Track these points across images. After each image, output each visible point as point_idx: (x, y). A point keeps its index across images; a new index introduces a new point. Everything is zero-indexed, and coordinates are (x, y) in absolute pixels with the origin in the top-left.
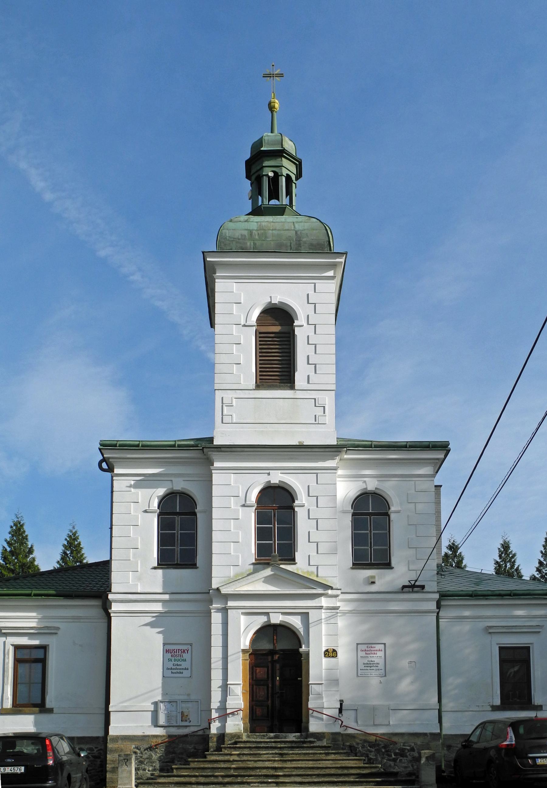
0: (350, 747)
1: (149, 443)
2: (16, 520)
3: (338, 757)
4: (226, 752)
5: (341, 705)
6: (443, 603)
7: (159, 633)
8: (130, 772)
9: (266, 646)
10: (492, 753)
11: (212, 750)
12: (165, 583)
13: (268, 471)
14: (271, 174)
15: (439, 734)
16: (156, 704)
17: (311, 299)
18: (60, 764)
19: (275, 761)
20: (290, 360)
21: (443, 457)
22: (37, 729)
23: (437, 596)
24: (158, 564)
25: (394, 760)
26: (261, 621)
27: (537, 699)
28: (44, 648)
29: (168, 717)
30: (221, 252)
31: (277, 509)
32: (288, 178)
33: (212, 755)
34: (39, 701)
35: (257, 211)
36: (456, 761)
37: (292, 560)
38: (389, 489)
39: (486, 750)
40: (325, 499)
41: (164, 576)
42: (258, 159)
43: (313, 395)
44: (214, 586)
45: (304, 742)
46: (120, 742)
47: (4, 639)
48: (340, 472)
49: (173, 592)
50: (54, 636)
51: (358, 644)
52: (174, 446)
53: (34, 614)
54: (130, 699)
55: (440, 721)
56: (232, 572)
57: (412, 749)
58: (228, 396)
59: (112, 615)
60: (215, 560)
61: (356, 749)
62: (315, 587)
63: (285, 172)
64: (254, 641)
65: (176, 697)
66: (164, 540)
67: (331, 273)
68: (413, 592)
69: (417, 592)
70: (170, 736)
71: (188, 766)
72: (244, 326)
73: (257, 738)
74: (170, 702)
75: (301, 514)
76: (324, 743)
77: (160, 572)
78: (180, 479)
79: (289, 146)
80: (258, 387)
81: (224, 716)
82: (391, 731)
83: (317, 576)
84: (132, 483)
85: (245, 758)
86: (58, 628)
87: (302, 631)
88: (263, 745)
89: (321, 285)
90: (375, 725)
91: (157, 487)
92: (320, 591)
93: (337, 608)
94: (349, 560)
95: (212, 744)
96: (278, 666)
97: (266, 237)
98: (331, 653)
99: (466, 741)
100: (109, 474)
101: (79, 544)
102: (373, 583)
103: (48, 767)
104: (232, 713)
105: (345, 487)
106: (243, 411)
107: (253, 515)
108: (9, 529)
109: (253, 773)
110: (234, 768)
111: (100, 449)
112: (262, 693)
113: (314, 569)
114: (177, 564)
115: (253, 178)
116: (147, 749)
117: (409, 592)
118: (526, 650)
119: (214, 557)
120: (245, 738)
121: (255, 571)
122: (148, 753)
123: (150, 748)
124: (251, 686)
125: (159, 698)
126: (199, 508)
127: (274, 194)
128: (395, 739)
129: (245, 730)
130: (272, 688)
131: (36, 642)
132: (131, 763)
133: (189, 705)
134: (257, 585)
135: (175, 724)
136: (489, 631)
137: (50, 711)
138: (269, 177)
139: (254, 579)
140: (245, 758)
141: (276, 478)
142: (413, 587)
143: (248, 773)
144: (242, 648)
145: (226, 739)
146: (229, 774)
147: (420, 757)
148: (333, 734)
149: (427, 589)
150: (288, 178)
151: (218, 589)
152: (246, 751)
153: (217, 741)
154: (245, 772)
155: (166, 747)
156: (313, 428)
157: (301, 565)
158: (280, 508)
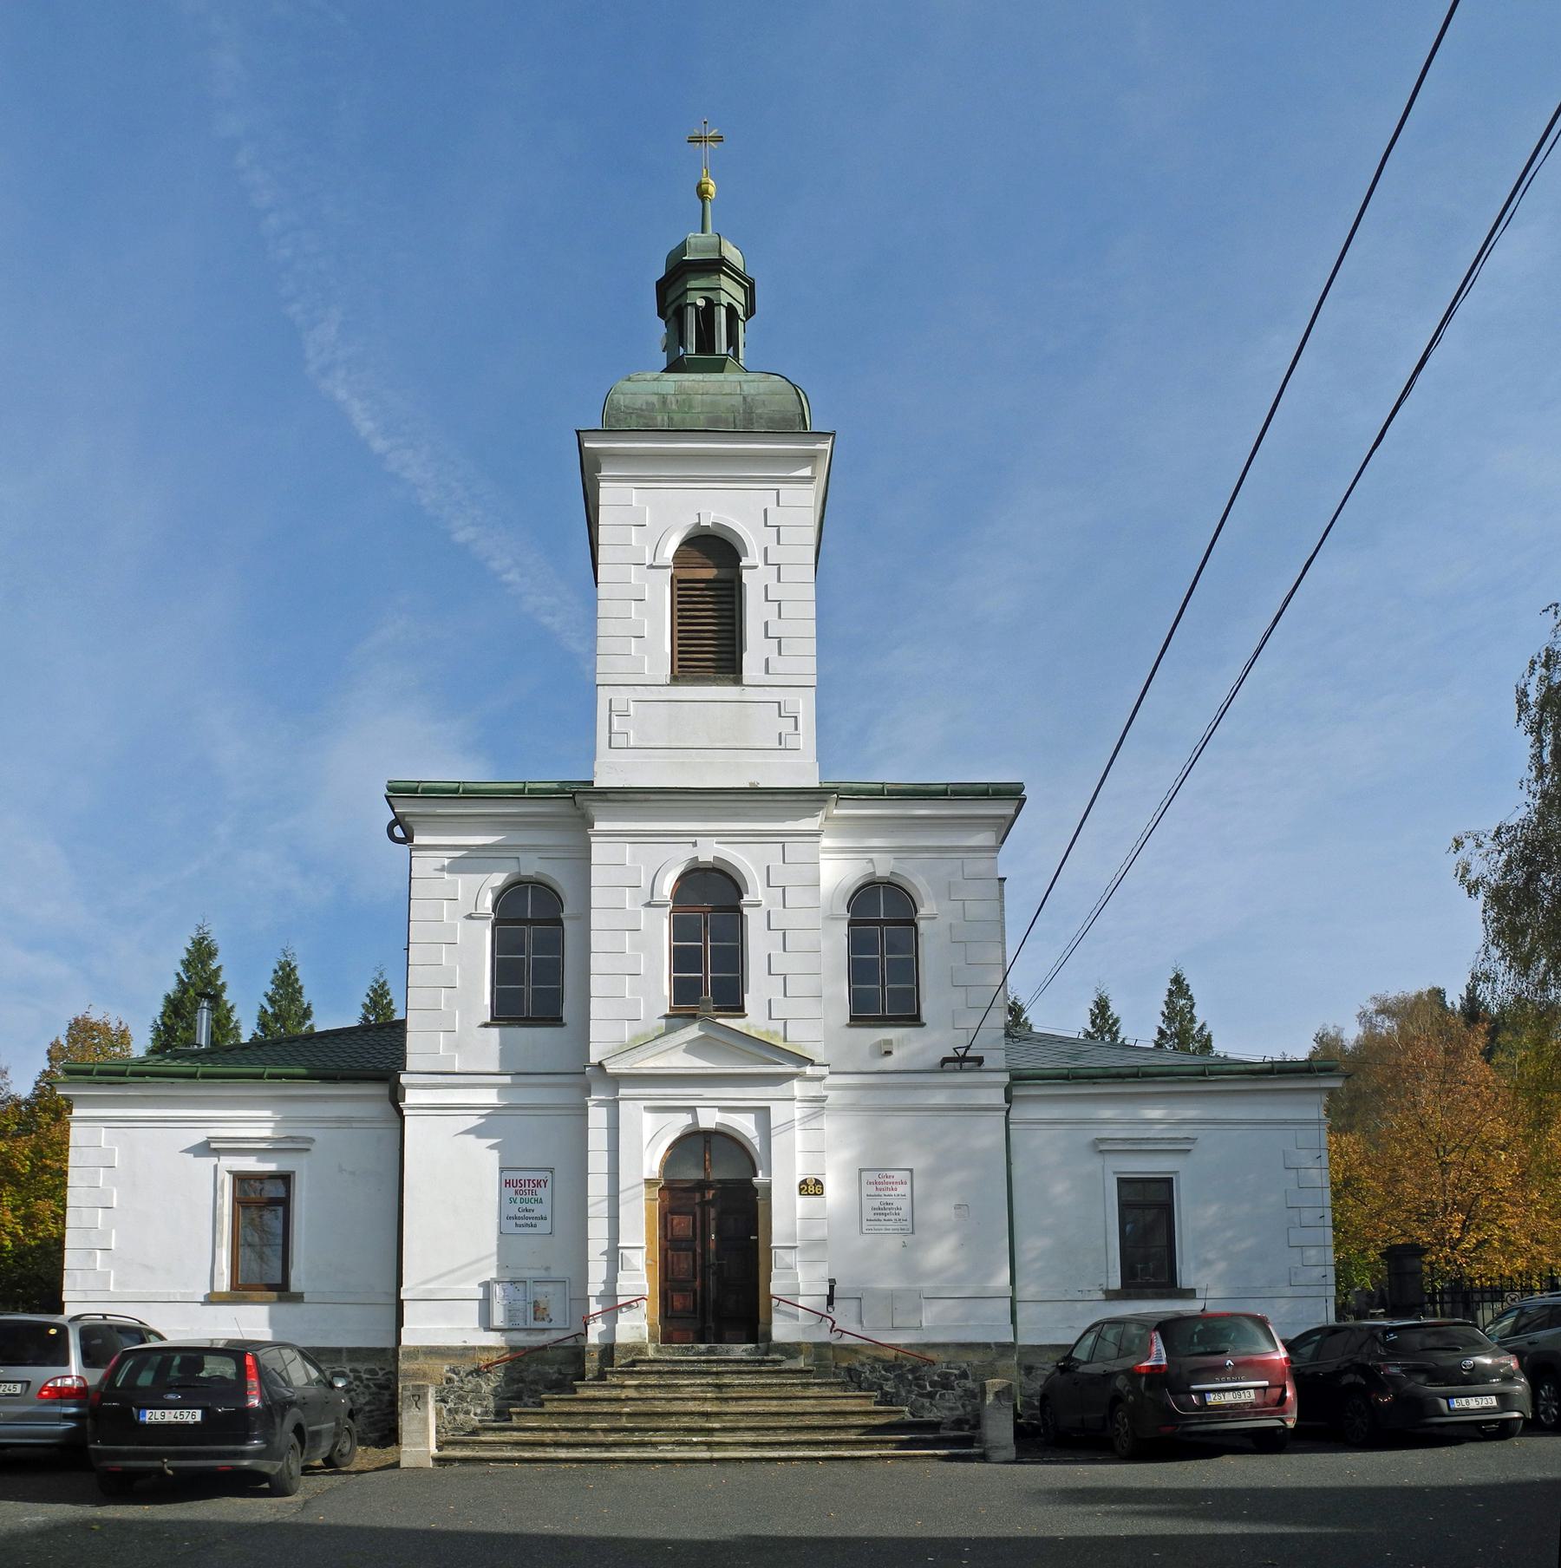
0: (849, 1370)
1: (476, 786)
2: (283, 959)
3: (827, 1392)
4: (615, 1381)
5: (832, 1288)
6: (1016, 1092)
7: (491, 1147)
8: (425, 1421)
9: (693, 1174)
10: (1121, 1383)
11: (590, 1376)
12: (505, 1053)
13: (693, 839)
14: (701, 303)
15: (1012, 1346)
16: (486, 1286)
17: (774, 520)
18: (277, 1407)
19: (706, 1399)
20: (733, 631)
21: (1012, 812)
22: (275, 1332)
23: (1005, 1078)
24: (493, 1018)
25: (931, 1396)
26: (681, 1122)
27: (1187, 1276)
28: (285, 1178)
29: (510, 1312)
30: (609, 431)
31: (710, 908)
32: (731, 310)
33: (588, 1386)
34: (278, 1280)
35: (676, 365)
36: (1044, 1398)
37: (738, 1009)
38: (920, 882)
39: (1108, 1377)
40: (800, 890)
41: (503, 1041)
42: (680, 271)
43: (776, 695)
44: (594, 1059)
45: (762, 1362)
46: (421, 1358)
47: (214, 1160)
48: (826, 842)
49: (517, 1072)
50: (305, 1155)
51: (861, 1170)
52: (522, 791)
53: (268, 1113)
54: (440, 1276)
55: (1014, 1321)
56: (627, 1032)
57: (964, 1375)
58: (621, 697)
59: (405, 1112)
60: (596, 1008)
61: (859, 1374)
62: (777, 1061)
63: (725, 299)
64: (669, 1163)
65: (526, 1274)
66: (504, 972)
67: (806, 472)
68: (961, 1070)
69: (969, 1070)
70: (512, 1349)
71: (539, 1410)
72: (651, 567)
73: (673, 1353)
74: (512, 1282)
75: (754, 921)
76: (801, 1363)
77: (495, 1031)
78: (533, 856)
79: (732, 254)
80: (675, 680)
81: (612, 1310)
82: (925, 1340)
83: (785, 1040)
84: (446, 862)
85: (650, 1393)
86: (311, 1140)
87: (756, 1142)
88: (685, 1368)
89: (789, 492)
90: (894, 1328)
91: (490, 871)
92: (790, 1068)
93: (822, 1099)
94: (843, 1011)
95: (591, 1365)
96: (713, 1213)
97: (690, 407)
98: (811, 1187)
99: (1066, 1360)
100: (405, 848)
101: (390, 1003)
102: (888, 1053)
103: (246, 1412)
104: (628, 1305)
105: (836, 865)
106: (647, 725)
107: (666, 922)
108: (272, 975)
109: (663, 1425)
110: (629, 1414)
111: (387, 797)
112: (684, 1264)
113: (779, 1026)
114: (527, 1019)
115: (670, 312)
116: (470, 1373)
117: (955, 1071)
118: (1167, 1183)
119: (594, 1002)
120: (651, 1354)
121: (670, 1030)
122: (474, 1380)
123: (477, 1372)
124: (664, 1252)
125: (493, 1274)
126: (568, 911)
127: (706, 341)
128: (931, 1355)
129: (652, 1338)
130: (703, 1255)
131: (271, 1167)
132: (426, 1403)
133: (549, 1288)
134: (674, 1057)
135: (522, 1325)
136: (1101, 1148)
137: (298, 1298)
138: (697, 307)
139: (667, 1046)
140: (650, 1393)
141: (709, 851)
142: (962, 1061)
143: (653, 1425)
144: (646, 1175)
145: (616, 1354)
146: (618, 1425)
147: (984, 1392)
148: (818, 1345)
149: (987, 1064)
150: (731, 310)
151: (600, 1064)
152: (652, 1380)
153: (601, 1359)
154: (648, 1421)
155: (507, 1368)
156: (775, 758)
157: (754, 1021)
158: (715, 909)
